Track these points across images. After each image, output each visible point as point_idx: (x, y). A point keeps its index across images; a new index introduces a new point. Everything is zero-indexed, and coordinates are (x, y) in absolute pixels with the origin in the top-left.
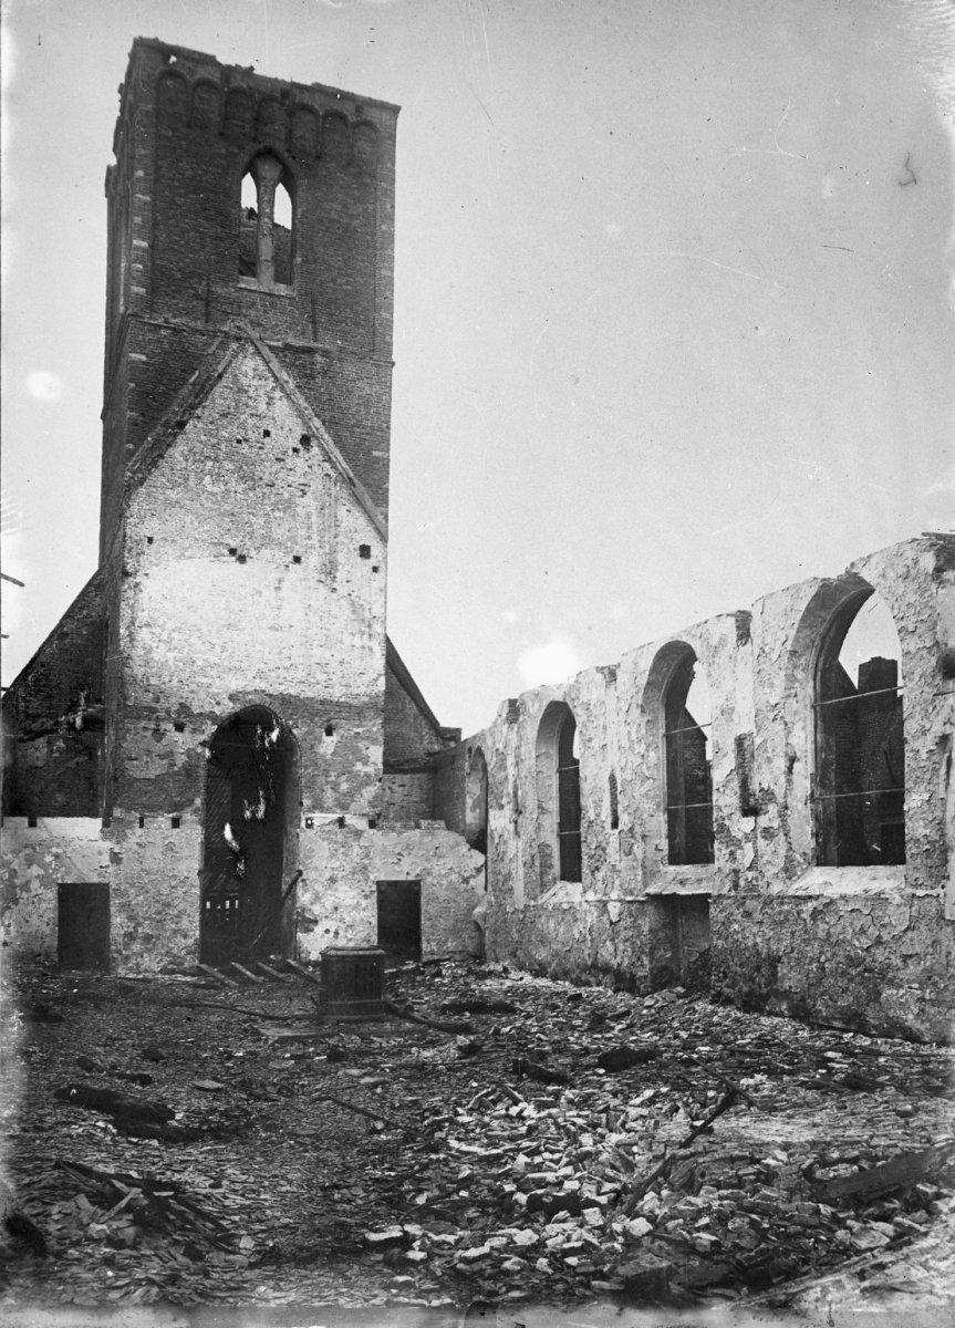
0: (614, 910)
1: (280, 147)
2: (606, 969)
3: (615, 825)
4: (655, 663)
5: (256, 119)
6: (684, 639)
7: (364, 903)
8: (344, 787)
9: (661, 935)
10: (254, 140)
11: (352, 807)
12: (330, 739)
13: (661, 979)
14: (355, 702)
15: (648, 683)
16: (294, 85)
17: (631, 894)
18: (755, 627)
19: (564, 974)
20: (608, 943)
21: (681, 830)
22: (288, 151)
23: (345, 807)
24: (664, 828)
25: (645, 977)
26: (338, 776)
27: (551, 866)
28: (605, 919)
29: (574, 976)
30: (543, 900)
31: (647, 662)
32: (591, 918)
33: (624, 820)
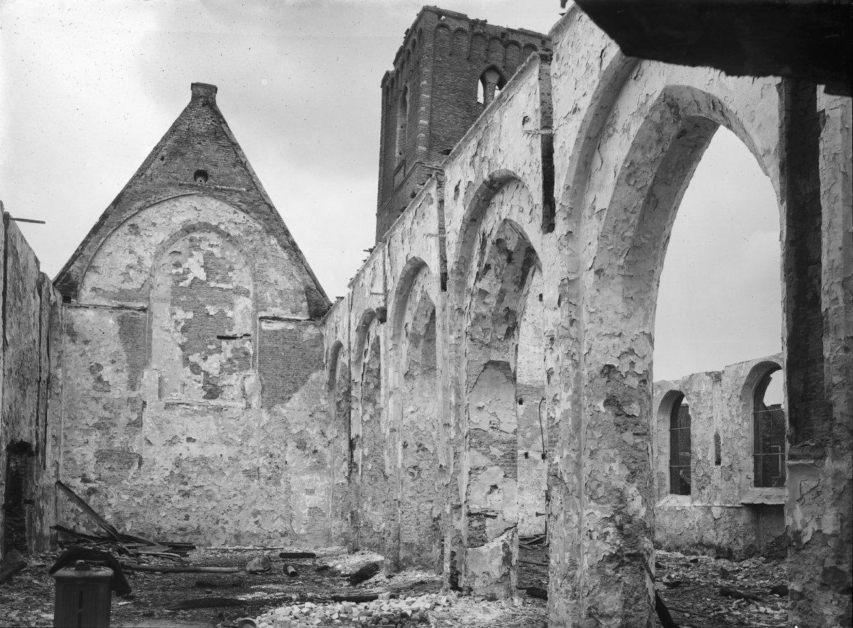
0: (716, 512)
1: (500, 65)
2: (710, 546)
3: (718, 462)
4: (750, 373)
5: (487, 50)
6: (774, 361)
7: (538, 503)
8: (528, 435)
9: (750, 527)
10: (486, 62)
11: (533, 446)
12: (521, 406)
13: (750, 552)
14: (535, 385)
15: (745, 384)
16: (509, 30)
17: (730, 502)
18: (544, 298)
19: (678, 548)
20: (711, 531)
21: (760, 469)
22: (504, 67)
23: (528, 446)
24: (752, 466)
25: (740, 551)
26: (525, 428)
27: (664, 486)
28: (709, 516)
29: (684, 549)
30: (660, 505)
31: (745, 372)
32: (699, 516)
33: (726, 461)
